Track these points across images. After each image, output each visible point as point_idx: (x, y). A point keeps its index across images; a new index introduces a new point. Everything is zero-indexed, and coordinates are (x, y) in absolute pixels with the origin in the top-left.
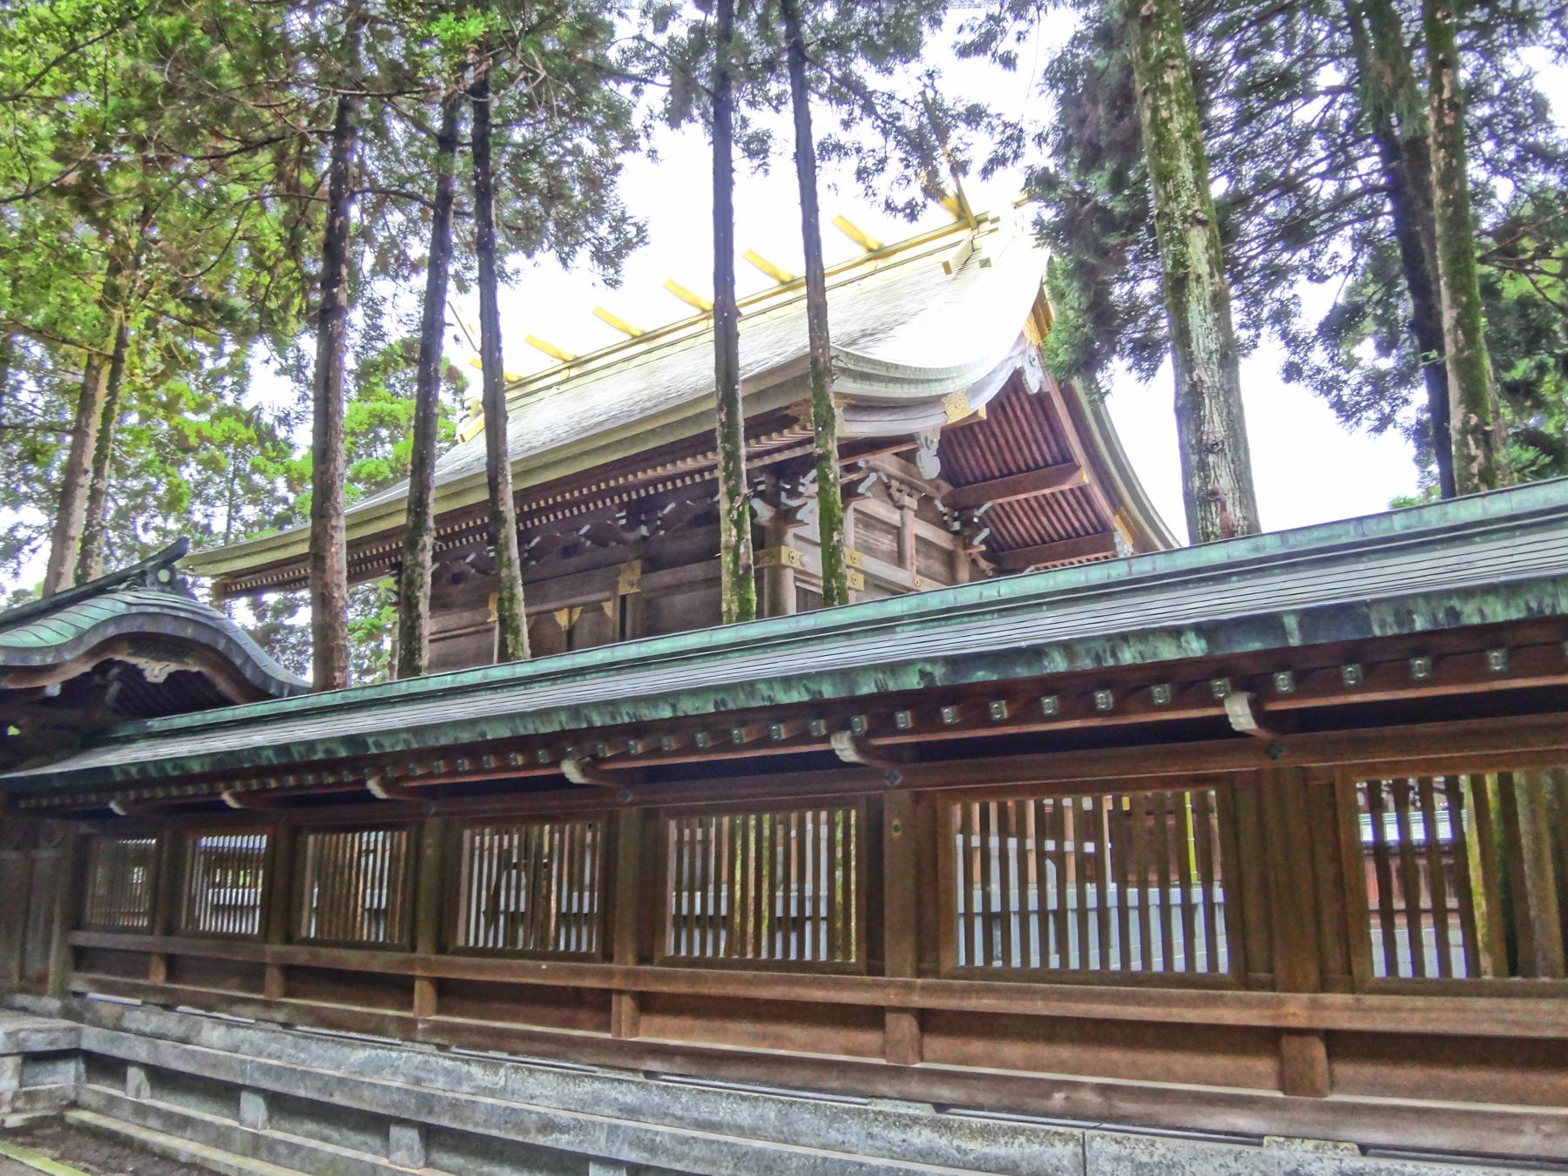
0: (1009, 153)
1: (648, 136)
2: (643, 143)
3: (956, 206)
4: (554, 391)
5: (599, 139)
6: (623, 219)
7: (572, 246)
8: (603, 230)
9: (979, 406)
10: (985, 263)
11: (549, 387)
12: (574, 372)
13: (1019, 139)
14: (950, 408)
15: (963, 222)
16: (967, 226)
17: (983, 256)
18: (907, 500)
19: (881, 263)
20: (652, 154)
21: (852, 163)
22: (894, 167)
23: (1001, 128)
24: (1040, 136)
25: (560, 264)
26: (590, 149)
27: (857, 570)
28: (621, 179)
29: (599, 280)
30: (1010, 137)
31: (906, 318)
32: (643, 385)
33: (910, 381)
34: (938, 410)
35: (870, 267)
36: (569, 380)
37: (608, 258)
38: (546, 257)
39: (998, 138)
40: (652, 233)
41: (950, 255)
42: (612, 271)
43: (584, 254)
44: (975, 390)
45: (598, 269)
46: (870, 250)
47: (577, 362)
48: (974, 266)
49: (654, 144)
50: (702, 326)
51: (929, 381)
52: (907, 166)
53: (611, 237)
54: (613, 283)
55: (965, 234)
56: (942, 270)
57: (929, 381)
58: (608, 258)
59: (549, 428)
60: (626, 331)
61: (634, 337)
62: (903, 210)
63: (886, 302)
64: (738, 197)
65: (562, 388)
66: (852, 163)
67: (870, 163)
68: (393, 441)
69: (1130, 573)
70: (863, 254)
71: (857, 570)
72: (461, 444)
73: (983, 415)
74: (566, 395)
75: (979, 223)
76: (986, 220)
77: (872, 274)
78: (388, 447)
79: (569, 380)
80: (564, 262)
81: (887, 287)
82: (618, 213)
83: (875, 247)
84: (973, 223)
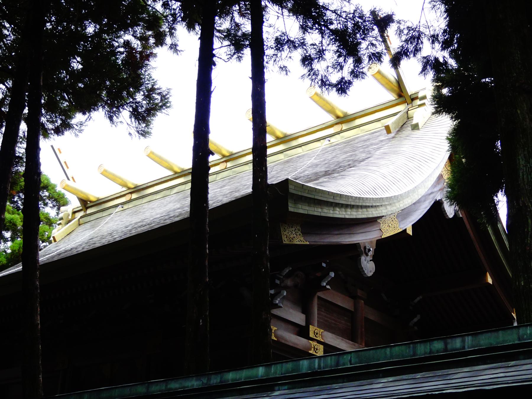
0: (411, 47)
1: (172, 34)
2: (168, 40)
3: (396, 89)
4: (119, 209)
5: (143, 39)
6: (152, 90)
7: (118, 108)
8: (139, 97)
9: (408, 226)
10: (416, 127)
11: (116, 206)
12: (134, 196)
13: (419, 38)
14: (384, 227)
15: (401, 100)
16: (405, 102)
17: (414, 122)
18: (359, 293)
19: (344, 127)
20: (174, 47)
21: (298, 54)
22: (330, 56)
23: (406, 32)
24: (433, 36)
25: (108, 120)
26: (136, 44)
27: (319, 342)
28: (152, 62)
29: (133, 131)
30: (413, 38)
31: (356, 164)
32: (178, 206)
33: (352, 207)
34: (375, 228)
35: (337, 128)
36: (131, 201)
37: (143, 116)
38: (99, 115)
39: (404, 38)
40: (172, 99)
41: (389, 122)
42: (144, 125)
43: (125, 113)
44: (404, 214)
45: (134, 123)
46: (338, 117)
47: (137, 189)
48: (408, 130)
49: (174, 41)
50: (212, 163)
51: (366, 207)
52: (339, 56)
53: (144, 102)
54: (144, 134)
55: (402, 108)
56: (385, 131)
57: (366, 207)
58: (143, 116)
59: (111, 234)
60: (171, 169)
61: (176, 173)
62: (335, 86)
63: (346, 153)
64: (216, 74)
65: (125, 207)
66: (298, 54)
67: (312, 52)
68: (13, 239)
69: (415, 354)
70: (330, 118)
71: (319, 342)
72: (54, 243)
73: (410, 232)
74: (127, 212)
75: (413, 100)
76: (417, 98)
77: (338, 133)
78: (9, 244)
79: (131, 201)
80: (111, 118)
81: (348, 143)
82: (150, 86)
83: (341, 115)
84: (409, 100)
